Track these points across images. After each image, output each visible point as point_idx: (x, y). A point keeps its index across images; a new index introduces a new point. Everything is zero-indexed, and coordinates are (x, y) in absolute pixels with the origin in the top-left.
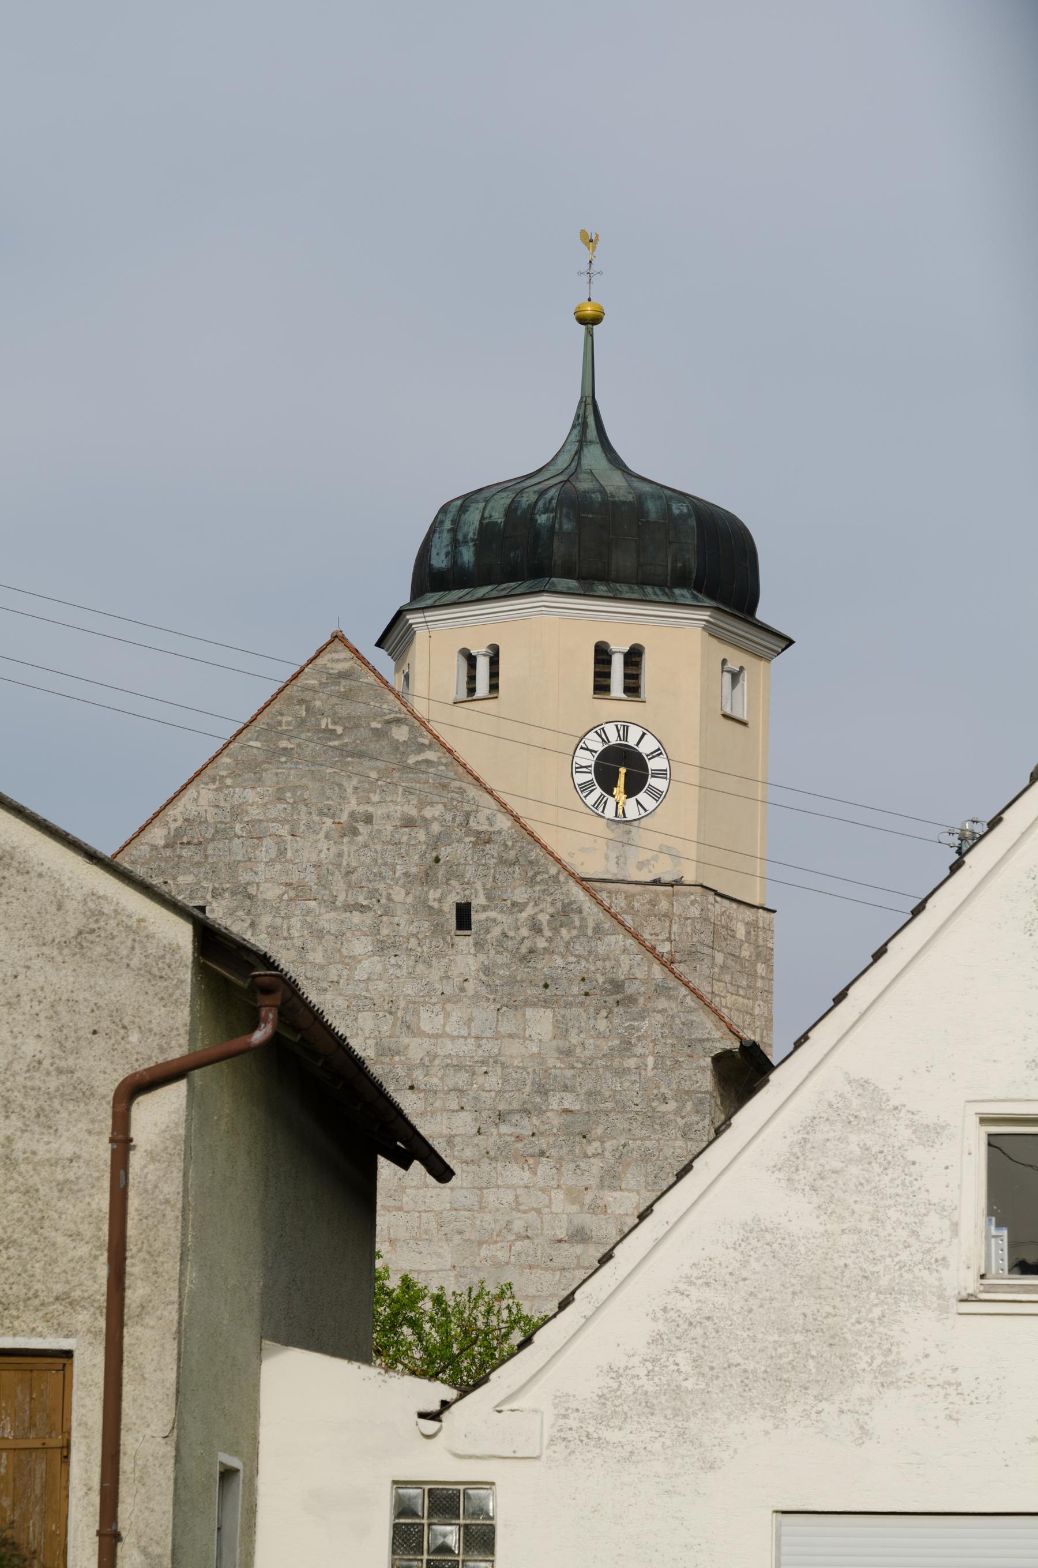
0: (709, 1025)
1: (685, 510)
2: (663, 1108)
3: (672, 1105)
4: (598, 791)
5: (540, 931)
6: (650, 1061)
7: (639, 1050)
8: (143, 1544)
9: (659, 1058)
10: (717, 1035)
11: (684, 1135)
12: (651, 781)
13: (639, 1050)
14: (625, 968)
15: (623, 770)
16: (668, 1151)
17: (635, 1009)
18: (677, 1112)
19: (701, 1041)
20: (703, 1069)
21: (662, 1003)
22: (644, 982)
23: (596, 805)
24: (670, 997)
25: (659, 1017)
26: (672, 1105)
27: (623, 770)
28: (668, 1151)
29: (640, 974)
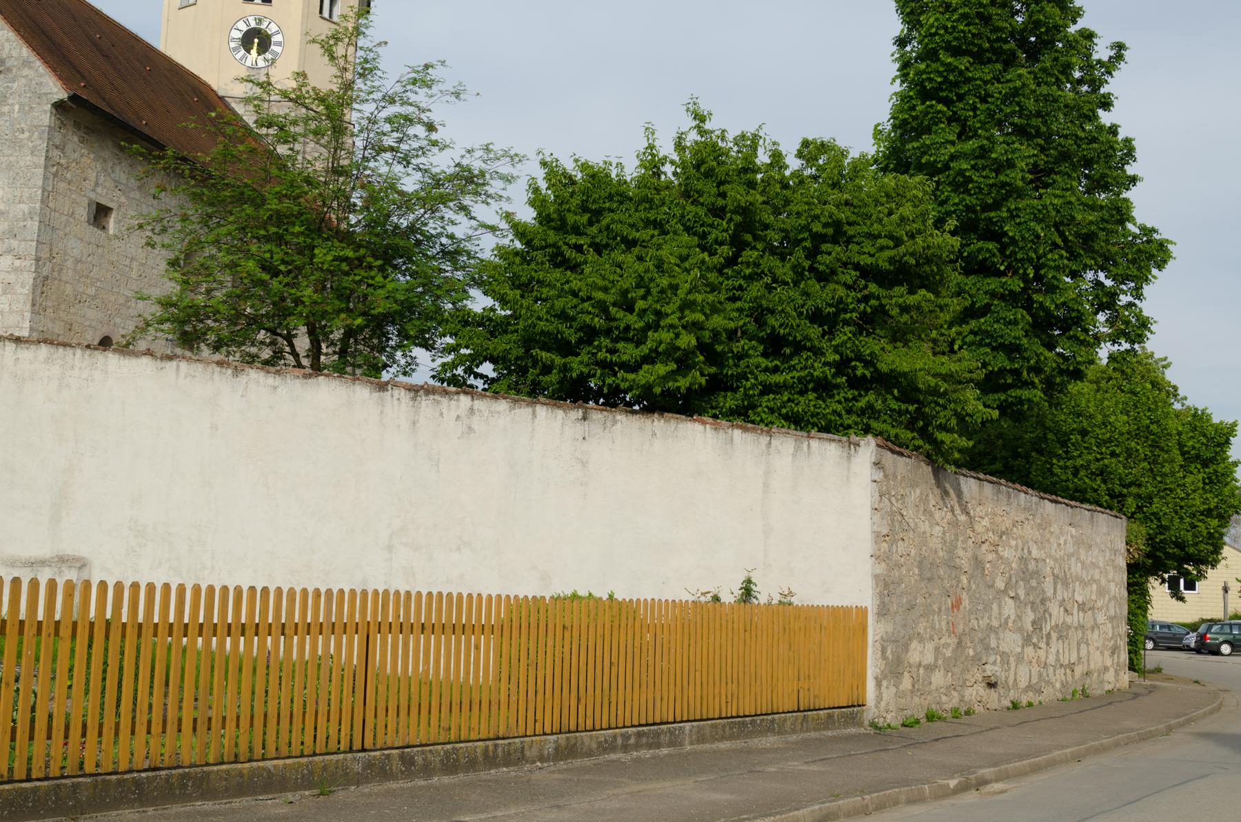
0: (51, 84)
1: (868, 375)
2: (22, 136)
3: (27, 134)
4: (243, 51)
5: (1030, 369)
6: (17, 107)
7: (11, 101)
8: (1161, 254)
9: (22, 105)
10: (55, 90)
11: (32, 153)
12: (273, 47)
13: (11, 101)
14: (7, 50)
15: (256, 41)
16: (22, 163)
17: (10, 76)
18: (29, 138)
19: (46, 94)
20: (45, 111)
21: (26, 72)
22: (17, 59)
23: (241, 59)
24: (30, 68)
25: (23, 81)
26: (27, 134)
27: (256, 41)
28: (22, 163)
29: (14, 54)
